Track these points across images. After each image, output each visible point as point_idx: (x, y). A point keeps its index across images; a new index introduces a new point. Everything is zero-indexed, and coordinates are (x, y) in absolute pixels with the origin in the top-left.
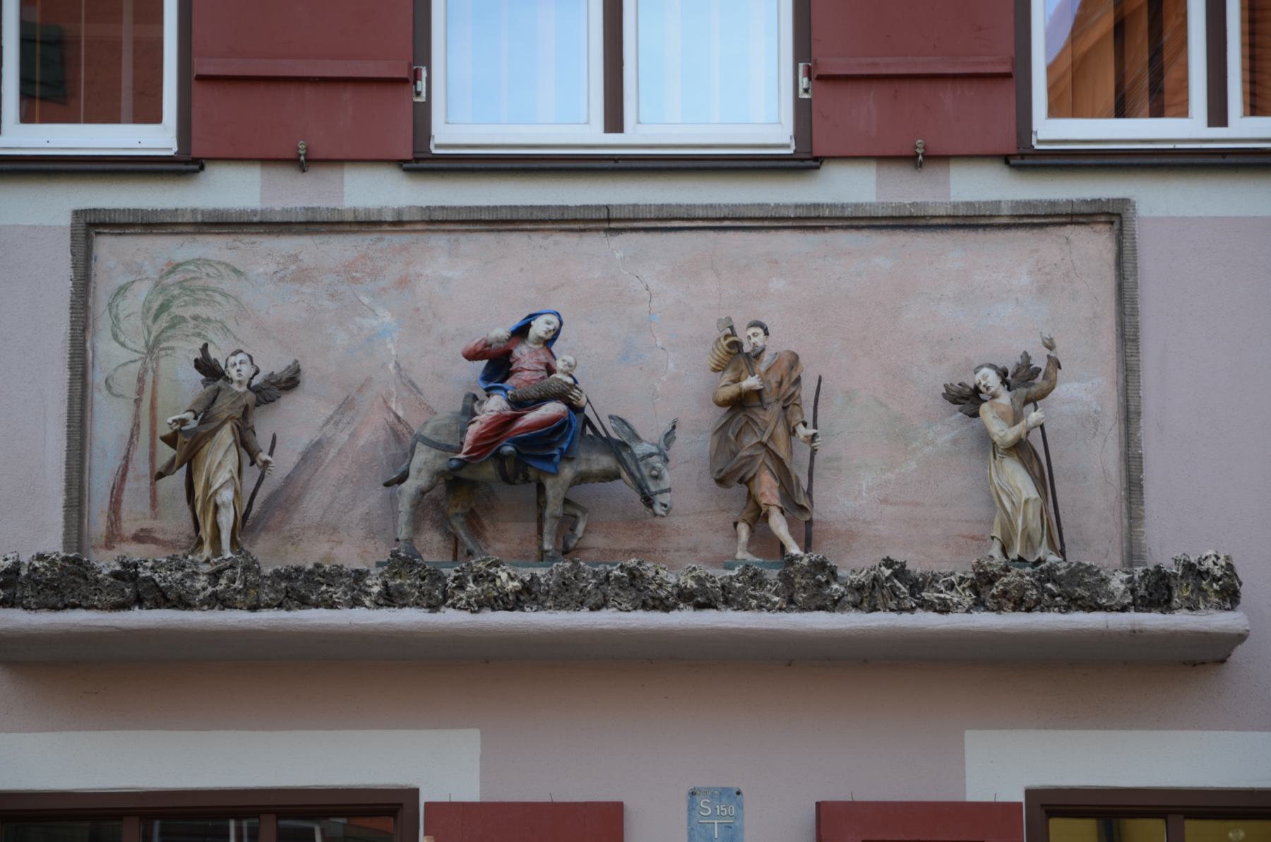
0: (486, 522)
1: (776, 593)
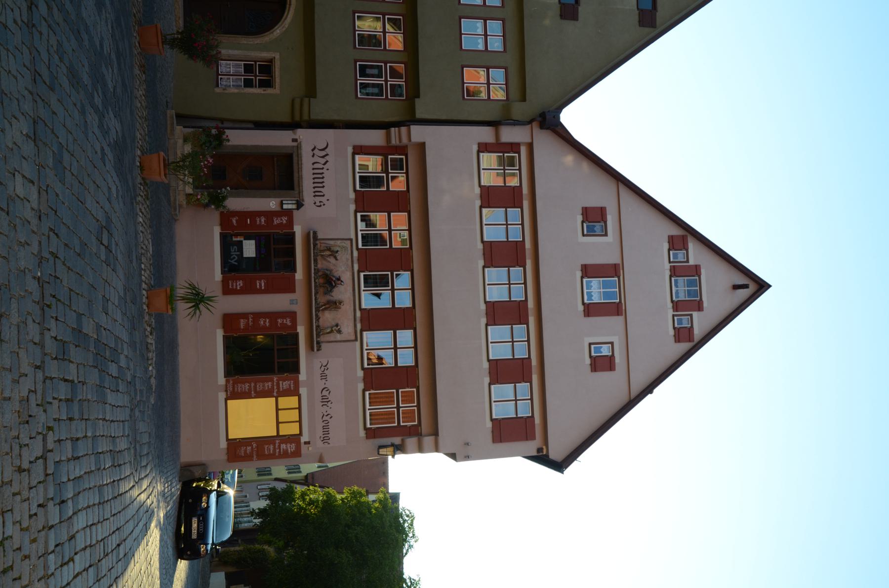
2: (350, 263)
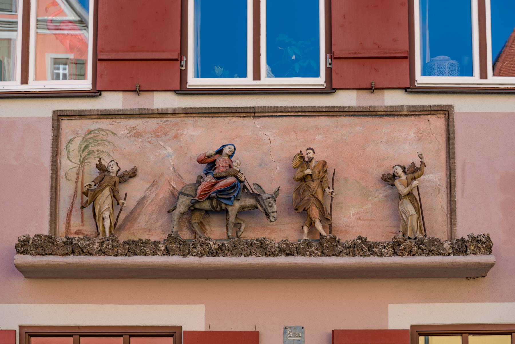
0: (207, 227)
1: (317, 250)
2: (153, 123)
